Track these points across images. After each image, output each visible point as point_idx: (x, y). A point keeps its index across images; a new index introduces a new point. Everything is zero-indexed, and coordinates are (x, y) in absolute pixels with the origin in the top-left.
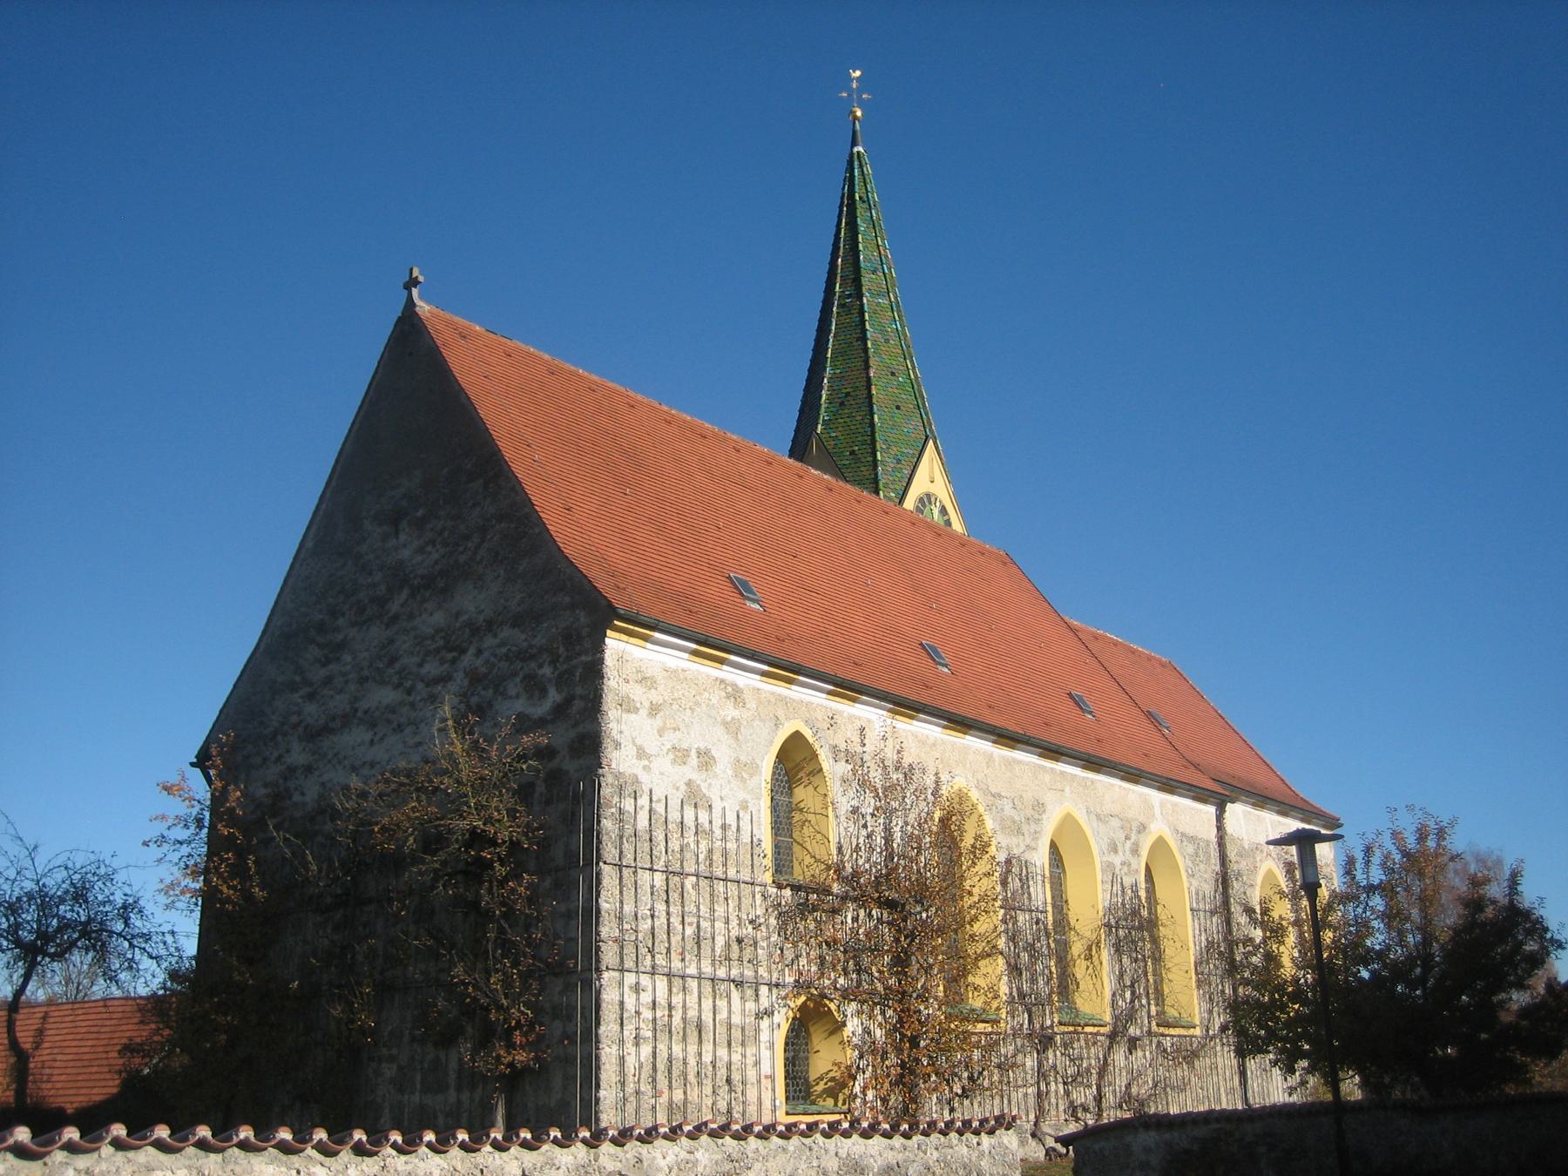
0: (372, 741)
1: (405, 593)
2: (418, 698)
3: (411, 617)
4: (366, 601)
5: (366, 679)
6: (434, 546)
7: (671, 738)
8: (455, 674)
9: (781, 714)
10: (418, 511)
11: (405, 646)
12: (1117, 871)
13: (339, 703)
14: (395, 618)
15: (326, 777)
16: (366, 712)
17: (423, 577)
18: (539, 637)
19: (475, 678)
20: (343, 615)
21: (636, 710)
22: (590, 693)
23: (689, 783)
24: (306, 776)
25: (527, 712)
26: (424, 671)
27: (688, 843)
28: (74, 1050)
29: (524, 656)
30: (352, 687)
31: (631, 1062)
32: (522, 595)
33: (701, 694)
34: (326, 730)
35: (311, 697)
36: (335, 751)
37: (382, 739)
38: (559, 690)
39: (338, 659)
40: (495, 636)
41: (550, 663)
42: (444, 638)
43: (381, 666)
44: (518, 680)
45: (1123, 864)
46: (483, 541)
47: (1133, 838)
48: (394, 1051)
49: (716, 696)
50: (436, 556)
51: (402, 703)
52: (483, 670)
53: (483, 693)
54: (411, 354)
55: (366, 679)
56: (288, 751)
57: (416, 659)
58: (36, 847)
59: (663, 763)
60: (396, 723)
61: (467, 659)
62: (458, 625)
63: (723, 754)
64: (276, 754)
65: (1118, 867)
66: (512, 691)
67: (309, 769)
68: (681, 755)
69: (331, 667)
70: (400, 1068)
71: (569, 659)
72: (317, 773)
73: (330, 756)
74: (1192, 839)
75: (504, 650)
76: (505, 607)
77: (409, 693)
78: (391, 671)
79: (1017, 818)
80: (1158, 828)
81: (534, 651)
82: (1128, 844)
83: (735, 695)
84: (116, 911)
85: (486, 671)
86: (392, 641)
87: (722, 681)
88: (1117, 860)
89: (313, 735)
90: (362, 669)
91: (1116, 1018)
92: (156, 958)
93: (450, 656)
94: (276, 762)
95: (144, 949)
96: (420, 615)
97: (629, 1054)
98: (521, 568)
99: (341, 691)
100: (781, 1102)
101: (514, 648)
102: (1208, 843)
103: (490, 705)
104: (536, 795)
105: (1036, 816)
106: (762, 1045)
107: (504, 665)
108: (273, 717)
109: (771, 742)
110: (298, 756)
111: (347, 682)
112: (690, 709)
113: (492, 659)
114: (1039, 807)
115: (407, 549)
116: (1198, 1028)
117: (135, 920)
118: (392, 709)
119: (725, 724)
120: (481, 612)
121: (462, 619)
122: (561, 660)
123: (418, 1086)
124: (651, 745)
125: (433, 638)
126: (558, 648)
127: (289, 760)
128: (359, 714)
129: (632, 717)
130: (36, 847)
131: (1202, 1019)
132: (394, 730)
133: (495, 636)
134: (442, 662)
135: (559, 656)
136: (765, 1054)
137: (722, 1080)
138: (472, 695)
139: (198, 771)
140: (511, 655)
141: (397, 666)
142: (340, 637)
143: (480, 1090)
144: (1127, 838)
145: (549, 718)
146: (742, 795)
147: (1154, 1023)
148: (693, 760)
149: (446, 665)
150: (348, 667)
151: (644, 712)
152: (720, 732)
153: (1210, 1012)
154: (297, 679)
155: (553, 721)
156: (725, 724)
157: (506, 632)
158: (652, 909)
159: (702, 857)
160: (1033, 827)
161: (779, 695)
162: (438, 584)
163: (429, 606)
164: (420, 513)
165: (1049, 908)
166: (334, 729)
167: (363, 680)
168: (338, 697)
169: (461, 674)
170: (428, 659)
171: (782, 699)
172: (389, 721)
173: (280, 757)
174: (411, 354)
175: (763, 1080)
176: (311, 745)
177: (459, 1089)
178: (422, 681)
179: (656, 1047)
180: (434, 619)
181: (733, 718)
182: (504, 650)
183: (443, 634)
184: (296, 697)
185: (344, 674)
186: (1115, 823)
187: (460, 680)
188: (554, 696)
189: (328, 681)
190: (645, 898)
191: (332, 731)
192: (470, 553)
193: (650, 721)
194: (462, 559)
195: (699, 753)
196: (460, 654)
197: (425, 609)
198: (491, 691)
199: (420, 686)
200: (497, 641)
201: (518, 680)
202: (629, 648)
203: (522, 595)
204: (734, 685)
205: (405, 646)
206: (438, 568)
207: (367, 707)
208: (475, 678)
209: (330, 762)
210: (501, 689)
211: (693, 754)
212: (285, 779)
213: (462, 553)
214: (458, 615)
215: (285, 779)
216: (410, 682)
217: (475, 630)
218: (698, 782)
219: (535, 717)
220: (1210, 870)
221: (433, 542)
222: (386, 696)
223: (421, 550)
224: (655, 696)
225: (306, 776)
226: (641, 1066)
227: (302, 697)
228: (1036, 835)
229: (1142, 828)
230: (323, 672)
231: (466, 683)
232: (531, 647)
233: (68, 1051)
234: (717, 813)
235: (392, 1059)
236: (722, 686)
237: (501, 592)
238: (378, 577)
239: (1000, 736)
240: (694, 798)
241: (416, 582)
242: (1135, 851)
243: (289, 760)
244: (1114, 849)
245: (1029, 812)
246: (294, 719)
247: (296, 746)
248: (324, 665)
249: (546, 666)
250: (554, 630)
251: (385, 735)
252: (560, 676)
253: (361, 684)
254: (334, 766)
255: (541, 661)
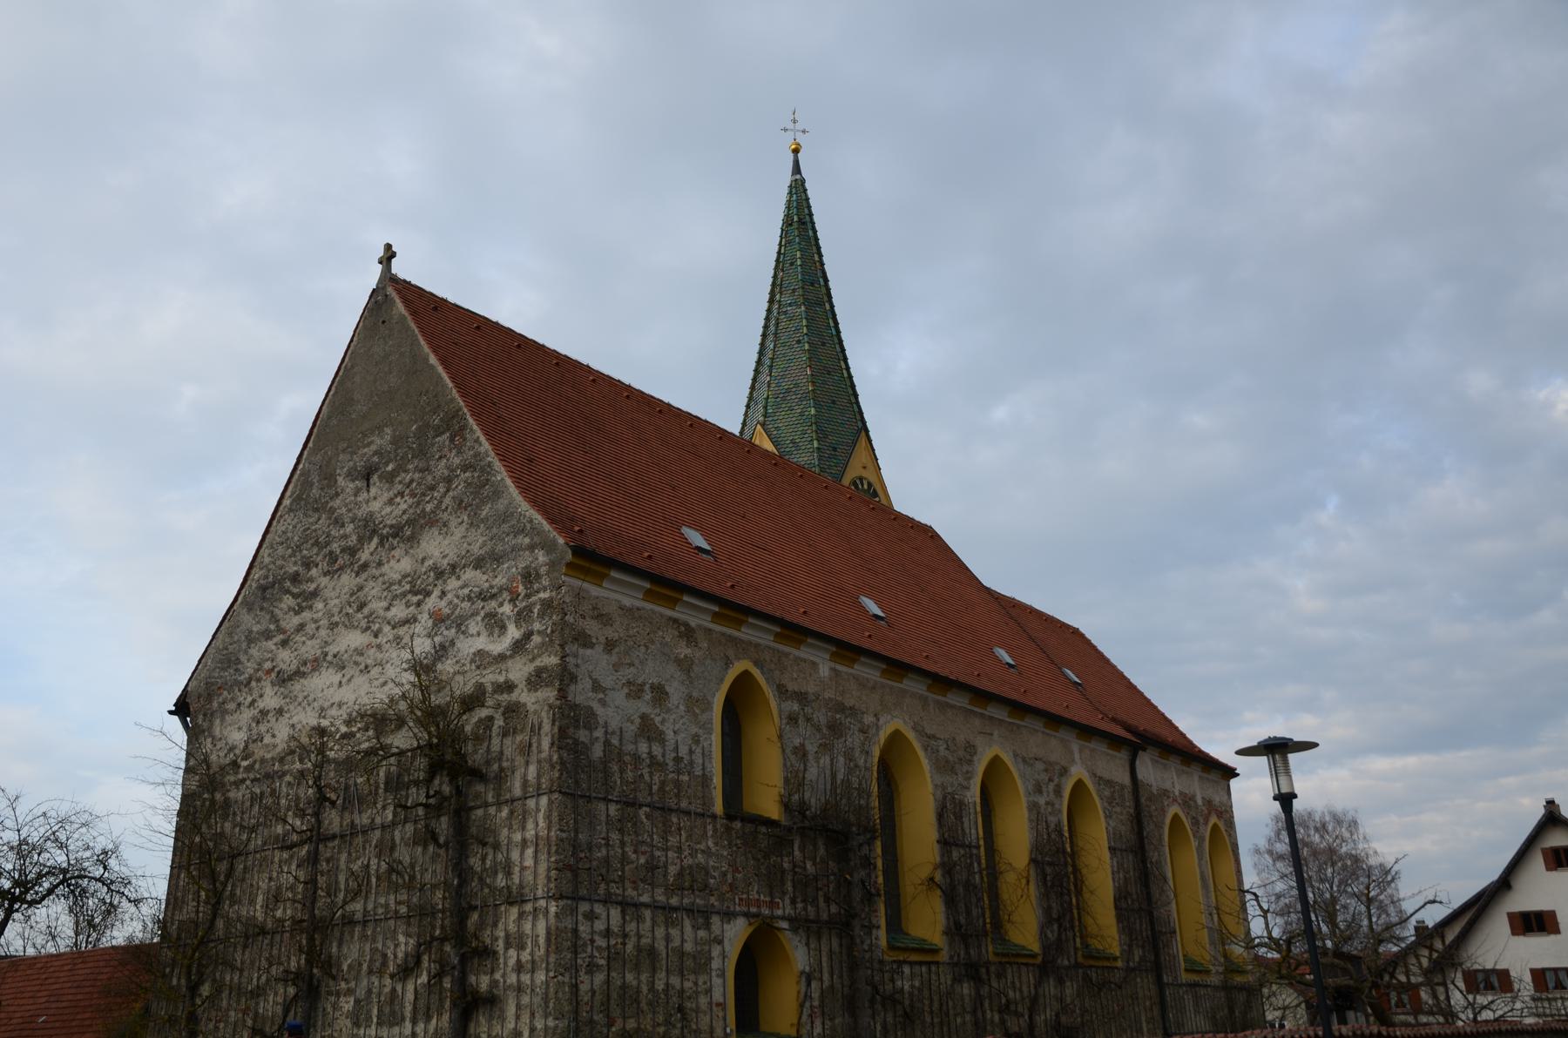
0: (340, 682)
1: (375, 540)
2: (385, 640)
3: (380, 564)
4: (338, 551)
5: (337, 624)
6: (403, 497)
7: (629, 673)
8: (419, 617)
9: (731, 653)
10: (387, 466)
11: (374, 592)
12: (1042, 811)
13: (310, 649)
14: (365, 566)
15: (295, 720)
16: (335, 656)
17: (392, 526)
18: (500, 577)
19: (439, 619)
20: (317, 566)
21: (592, 646)
22: (547, 629)
23: (644, 717)
24: (277, 720)
25: (487, 649)
26: (390, 614)
27: (642, 774)
28: (70, 997)
29: (484, 596)
30: (323, 632)
31: (584, 988)
32: (484, 538)
33: (655, 632)
34: (299, 674)
35: (284, 643)
36: (306, 694)
37: (349, 680)
38: (518, 626)
39: (311, 607)
40: (458, 578)
41: (510, 601)
42: (410, 582)
43: (351, 611)
44: (479, 618)
45: (1047, 803)
46: (448, 491)
47: (1056, 780)
48: (353, 984)
49: (669, 635)
50: (404, 506)
51: (369, 646)
52: (447, 611)
53: (445, 633)
54: (384, 322)
55: (337, 624)
56: (261, 696)
57: (384, 604)
58: (17, 798)
59: (619, 697)
60: (363, 665)
61: (432, 602)
62: (424, 570)
63: (676, 692)
64: (250, 699)
65: (1043, 807)
66: (473, 629)
67: (280, 712)
68: (635, 691)
69: (304, 614)
70: (357, 1002)
71: (528, 596)
72: (287, 715)
73: (300, 699)
74: (1109, 783)
75: (466, 591)
76: (468, 551)
77: (376, 636)
78: (360, 615)
79: (951, 758)
80: (1078, 771)
81: (494, 591)
82: (1051, 786)
83: (688, 634)
84: (96, 858)
85: (449, 612)
86: (361, 588)
87: (675, 621)
88: (1042, 801)
89: (284, 679)
90: (333, 616)
91: (1046, 948)
92: (135, 901)
93: (415, 599)
94: (249, 707)
95: (123, 893)
96: (388, 562)
97: (582, 982)
98: (484, 513)
99: (313, 637)
100: (731, 1030)
101: (476, 589)
102: (1123, 787)
103: (452, 643)
104: (495, 727)
105: (968, 757)
106: (714, 974)
107: (466, 605)
108: (249, 664)
109: (722, 680)
110: (270, 700)
111: (318, 628)
112: (646, 646)
113: (456, 601)
114: (971, 749)
115: (380, 503)
116: (1119, 960)
117: (112, 862)
118: (359, 652)
119: (679, 662)
120: (444, 557)
121: (426, 564)
122: (520, 598)
123: (375, 1020)
124: (607, 682)
125: (400, 583)
126: (517, 587)
127: (261, 704)
128: (329, 658)
129: (589, 652)
130: (17, 798)
131: (1122, 951)
132: (361, 671)
133: (458, 578)
134: (408, 605)
135: (519, 595)
136: (717, 981)
137: (674, 1008)
138: (436, 634)
139: (176, 718)
140: (473, 595)
141: (366, 611)
142: (312, 587)
143: (434, 1021)
144: (1050, 780)
145: (508, 653)
146: (694, 730)
147: (1080, 953)
148: (648, 696)
149: (411, 608)
150: (320, 614)
151: (599, 648)
152: (672, 669)
153: (1130, 946)
154: (272, 627)
155: (511, 657)
156: (679, 662)
157: (469, 574)
158: (607, 839)
159: (655, 788)
160: (965, 768)
161: (730, 636)
162: (405, 533)
163: (396, 553)
164: (390, 468)
165: (982, 842)
166: (304, 673)
167: (333, 626)
168: (309, 643)
169: (426, 616)
170: (395, 602)
171: (731, 639)
172: (356, 663)
173: (254, 701)
174: (384, 322)
175: (714, 1008)
176: (282, 689)
177: (414, 1022)
178: (389, 623)
179: (609, 975)
180: (400, 564)
181: (686, 656)
182: (466, 591)
183: (409, 579)
184: (270, 644)
185: (316, 621)
186: (1040, 766)
187: (425, 621)
188: (513, 633)
189: (301, 627)
190: (602, 828)
191: (303, 675)
192: (436, 502)
193: (605, 657)
194: (428, 508)
195: (652, 687)
196: (424, 598)
197: (393, 556)
198: (453, 630)
199: (387, 629)
200: (460, 583)
201: (479, 618)
202: (586, 585)
203: (484, 538)
204: (686, 625)
205: (374, 592)
206: (405, 517)
207: (335, 651)
208: (439, 619)
209: (300, 704)
210: (463, 628)
211: (647, 687)
212: (258, 722)
213: (428, 502)
214: (423, 560)
215: (258, 722)
216: (377, 625)
217: (440, 574)
218: (652, 716)
219: (495, 653)
220: (1125, 812)
221: (401, 494)
222: (353, 639)
223: (390, 502)
224: (610, 633)
225: (277, 720)
226: (593, 992)
227: (276, 644)
228: (969, 776)
229: (1064, 772)
230: (296, 620)
231: (430, 623)
232: (492, 587)
233: (65, 998)
234: (670, 745)
235: (350, 992)
236: (675, 626)
237: (465, 537)
238: (349, 528)
239: (889, 785)
240: (648, 730)
241: (385, 532)
242: (1058, 791)
243: (261, 704)
244: (1038, 790)
245: (961, 753)
246: (268, 665)
247: (269, 691)
248: (297, 613)
249: (506, 603)
250: (514, 570)
251: (352, 676)
252: (519, 614)
253: (332, 629)
254: (304, 708)
255: (500, 600)
